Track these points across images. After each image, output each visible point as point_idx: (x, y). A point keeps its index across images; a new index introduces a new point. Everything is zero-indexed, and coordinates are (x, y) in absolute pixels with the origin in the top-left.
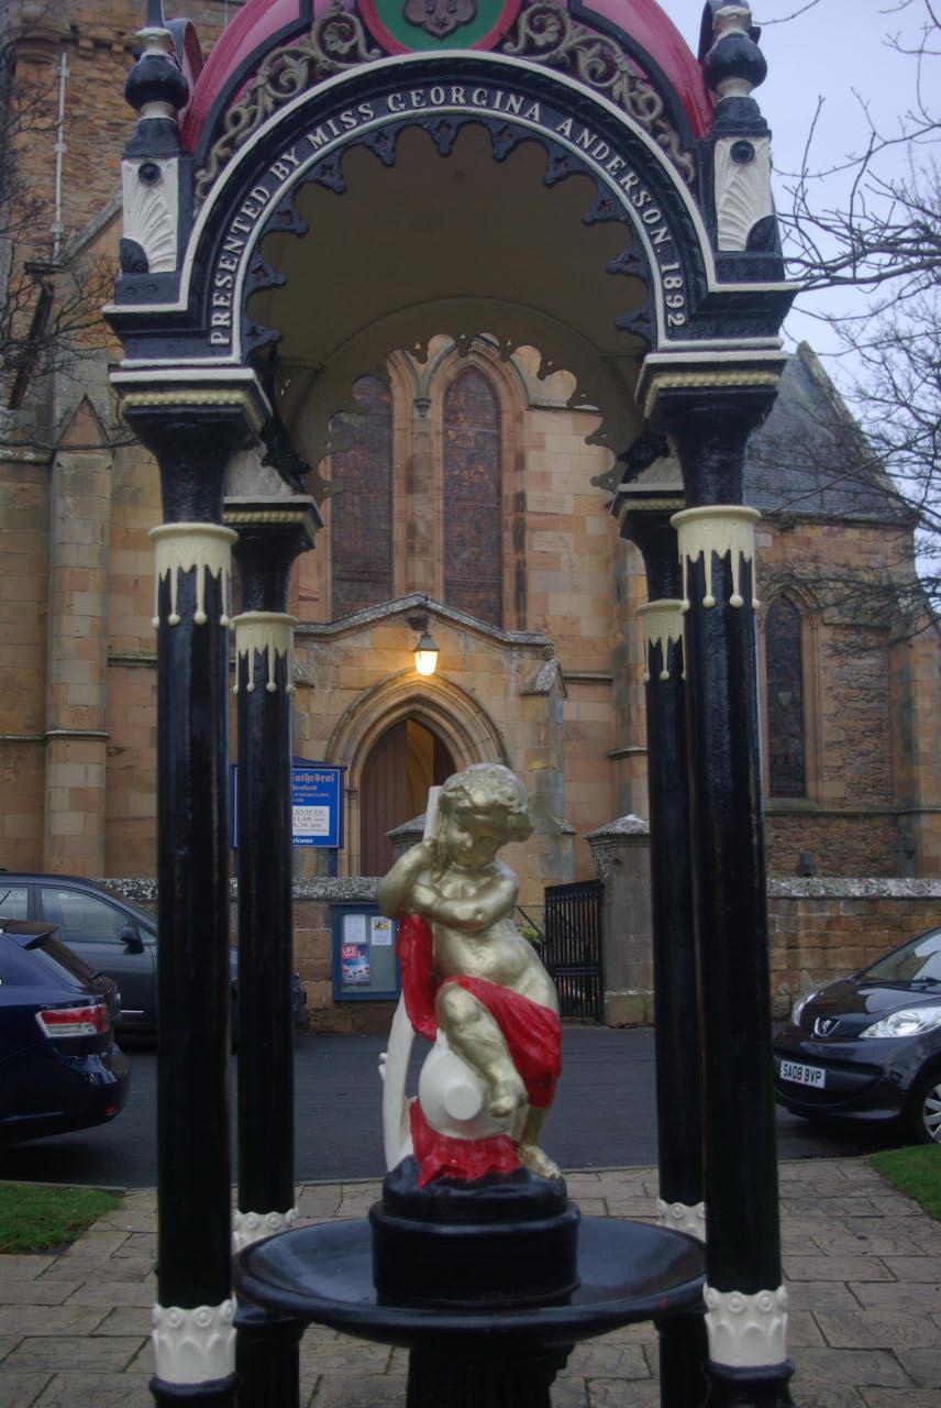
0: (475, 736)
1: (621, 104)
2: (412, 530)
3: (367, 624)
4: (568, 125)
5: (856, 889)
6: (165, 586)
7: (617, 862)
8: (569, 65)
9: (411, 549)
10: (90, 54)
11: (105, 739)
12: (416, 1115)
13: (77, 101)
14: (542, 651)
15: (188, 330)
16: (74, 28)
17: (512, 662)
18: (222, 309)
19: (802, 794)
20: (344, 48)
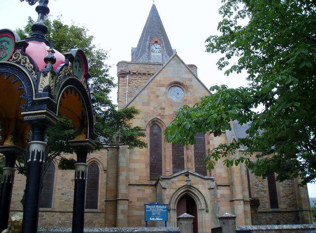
0: (200, 198)
2: (188, 157)
7: (224, 223)
8: (19, 63)
9: (188, 161)
11: (128, 200)
13: (130, 83)
14: (212, 180)
16: (130, 71)
17: (206, 182)
19: (278, 207)
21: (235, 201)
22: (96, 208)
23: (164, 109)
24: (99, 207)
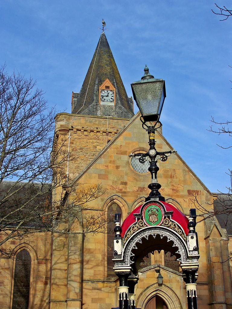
1: (177, 232)
6: (120, 295)
10: (76, 132)
13: (73, 143)
15: (123, 261)
21: (215, 305)
23: (126, 184)
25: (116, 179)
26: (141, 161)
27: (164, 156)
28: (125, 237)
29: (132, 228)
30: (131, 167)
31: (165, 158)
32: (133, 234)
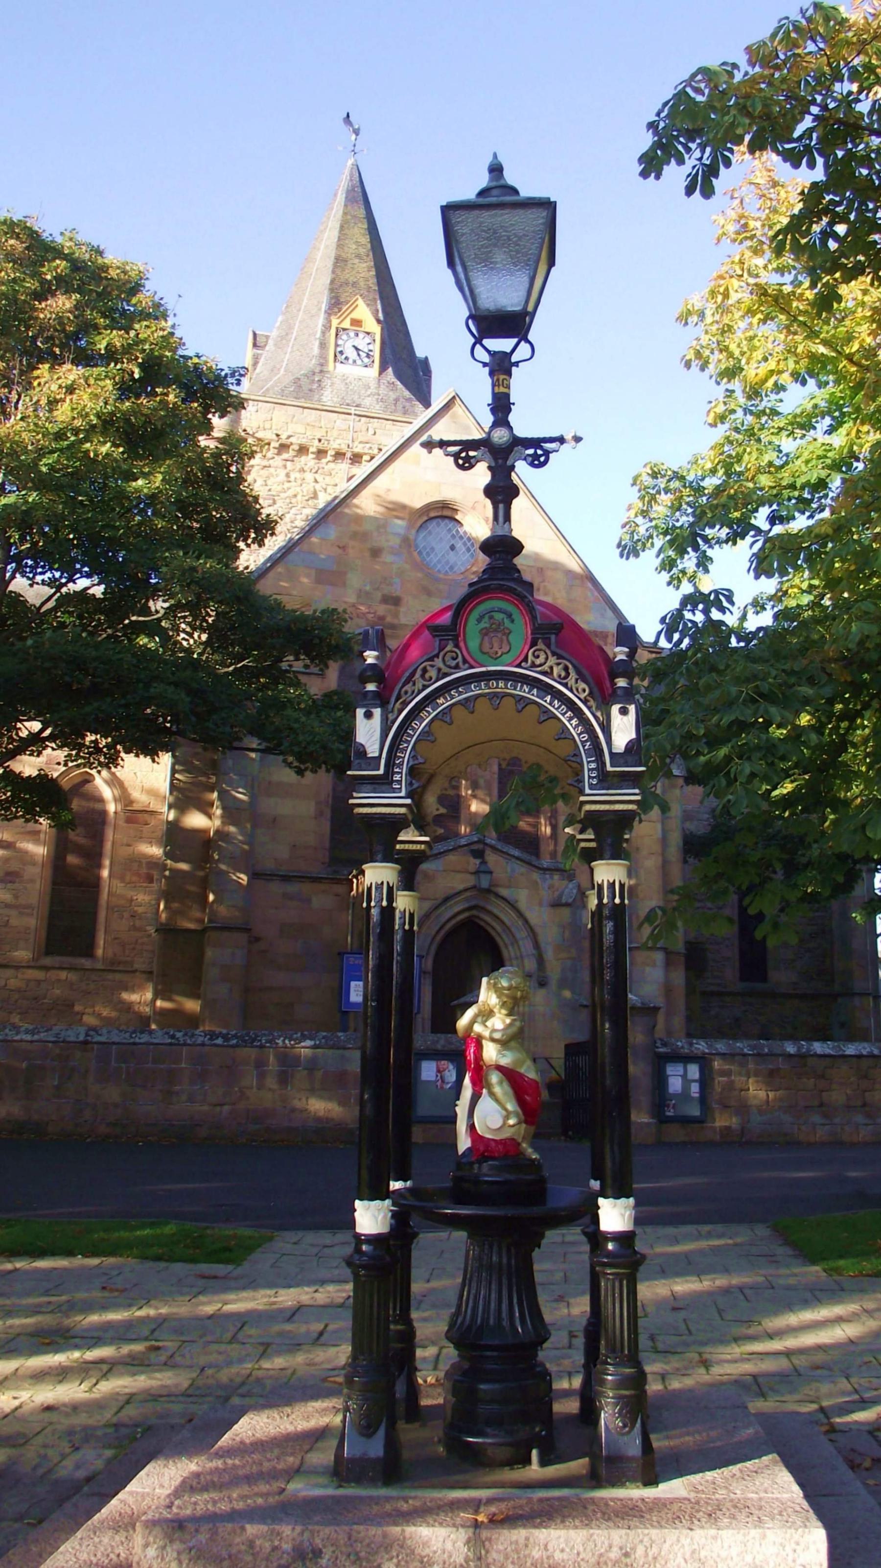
1: (571, 690)
3: (441, 853)
4: (548, 698)
5: (791, 1049)
12: (472, 1128)
15: (384, 782)
18: (398, 773)
19: (764, 978)
20: (453, 663)
22: (88, 951)
23: (396, 601)
24: (100, 952)
25: (368, 588)
26: (461, 462)
27: (539, 452)
28: (396, 701)
29: (419, 672)
30: (415, 554)
31: (542, 459)
32: (423, 690)
